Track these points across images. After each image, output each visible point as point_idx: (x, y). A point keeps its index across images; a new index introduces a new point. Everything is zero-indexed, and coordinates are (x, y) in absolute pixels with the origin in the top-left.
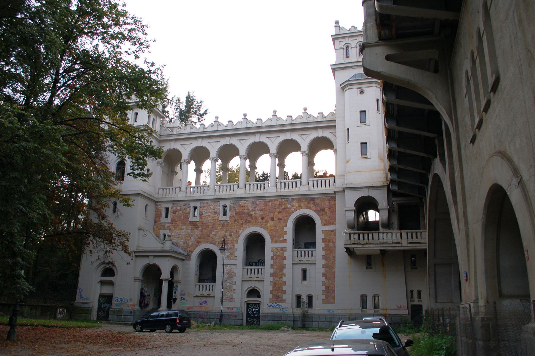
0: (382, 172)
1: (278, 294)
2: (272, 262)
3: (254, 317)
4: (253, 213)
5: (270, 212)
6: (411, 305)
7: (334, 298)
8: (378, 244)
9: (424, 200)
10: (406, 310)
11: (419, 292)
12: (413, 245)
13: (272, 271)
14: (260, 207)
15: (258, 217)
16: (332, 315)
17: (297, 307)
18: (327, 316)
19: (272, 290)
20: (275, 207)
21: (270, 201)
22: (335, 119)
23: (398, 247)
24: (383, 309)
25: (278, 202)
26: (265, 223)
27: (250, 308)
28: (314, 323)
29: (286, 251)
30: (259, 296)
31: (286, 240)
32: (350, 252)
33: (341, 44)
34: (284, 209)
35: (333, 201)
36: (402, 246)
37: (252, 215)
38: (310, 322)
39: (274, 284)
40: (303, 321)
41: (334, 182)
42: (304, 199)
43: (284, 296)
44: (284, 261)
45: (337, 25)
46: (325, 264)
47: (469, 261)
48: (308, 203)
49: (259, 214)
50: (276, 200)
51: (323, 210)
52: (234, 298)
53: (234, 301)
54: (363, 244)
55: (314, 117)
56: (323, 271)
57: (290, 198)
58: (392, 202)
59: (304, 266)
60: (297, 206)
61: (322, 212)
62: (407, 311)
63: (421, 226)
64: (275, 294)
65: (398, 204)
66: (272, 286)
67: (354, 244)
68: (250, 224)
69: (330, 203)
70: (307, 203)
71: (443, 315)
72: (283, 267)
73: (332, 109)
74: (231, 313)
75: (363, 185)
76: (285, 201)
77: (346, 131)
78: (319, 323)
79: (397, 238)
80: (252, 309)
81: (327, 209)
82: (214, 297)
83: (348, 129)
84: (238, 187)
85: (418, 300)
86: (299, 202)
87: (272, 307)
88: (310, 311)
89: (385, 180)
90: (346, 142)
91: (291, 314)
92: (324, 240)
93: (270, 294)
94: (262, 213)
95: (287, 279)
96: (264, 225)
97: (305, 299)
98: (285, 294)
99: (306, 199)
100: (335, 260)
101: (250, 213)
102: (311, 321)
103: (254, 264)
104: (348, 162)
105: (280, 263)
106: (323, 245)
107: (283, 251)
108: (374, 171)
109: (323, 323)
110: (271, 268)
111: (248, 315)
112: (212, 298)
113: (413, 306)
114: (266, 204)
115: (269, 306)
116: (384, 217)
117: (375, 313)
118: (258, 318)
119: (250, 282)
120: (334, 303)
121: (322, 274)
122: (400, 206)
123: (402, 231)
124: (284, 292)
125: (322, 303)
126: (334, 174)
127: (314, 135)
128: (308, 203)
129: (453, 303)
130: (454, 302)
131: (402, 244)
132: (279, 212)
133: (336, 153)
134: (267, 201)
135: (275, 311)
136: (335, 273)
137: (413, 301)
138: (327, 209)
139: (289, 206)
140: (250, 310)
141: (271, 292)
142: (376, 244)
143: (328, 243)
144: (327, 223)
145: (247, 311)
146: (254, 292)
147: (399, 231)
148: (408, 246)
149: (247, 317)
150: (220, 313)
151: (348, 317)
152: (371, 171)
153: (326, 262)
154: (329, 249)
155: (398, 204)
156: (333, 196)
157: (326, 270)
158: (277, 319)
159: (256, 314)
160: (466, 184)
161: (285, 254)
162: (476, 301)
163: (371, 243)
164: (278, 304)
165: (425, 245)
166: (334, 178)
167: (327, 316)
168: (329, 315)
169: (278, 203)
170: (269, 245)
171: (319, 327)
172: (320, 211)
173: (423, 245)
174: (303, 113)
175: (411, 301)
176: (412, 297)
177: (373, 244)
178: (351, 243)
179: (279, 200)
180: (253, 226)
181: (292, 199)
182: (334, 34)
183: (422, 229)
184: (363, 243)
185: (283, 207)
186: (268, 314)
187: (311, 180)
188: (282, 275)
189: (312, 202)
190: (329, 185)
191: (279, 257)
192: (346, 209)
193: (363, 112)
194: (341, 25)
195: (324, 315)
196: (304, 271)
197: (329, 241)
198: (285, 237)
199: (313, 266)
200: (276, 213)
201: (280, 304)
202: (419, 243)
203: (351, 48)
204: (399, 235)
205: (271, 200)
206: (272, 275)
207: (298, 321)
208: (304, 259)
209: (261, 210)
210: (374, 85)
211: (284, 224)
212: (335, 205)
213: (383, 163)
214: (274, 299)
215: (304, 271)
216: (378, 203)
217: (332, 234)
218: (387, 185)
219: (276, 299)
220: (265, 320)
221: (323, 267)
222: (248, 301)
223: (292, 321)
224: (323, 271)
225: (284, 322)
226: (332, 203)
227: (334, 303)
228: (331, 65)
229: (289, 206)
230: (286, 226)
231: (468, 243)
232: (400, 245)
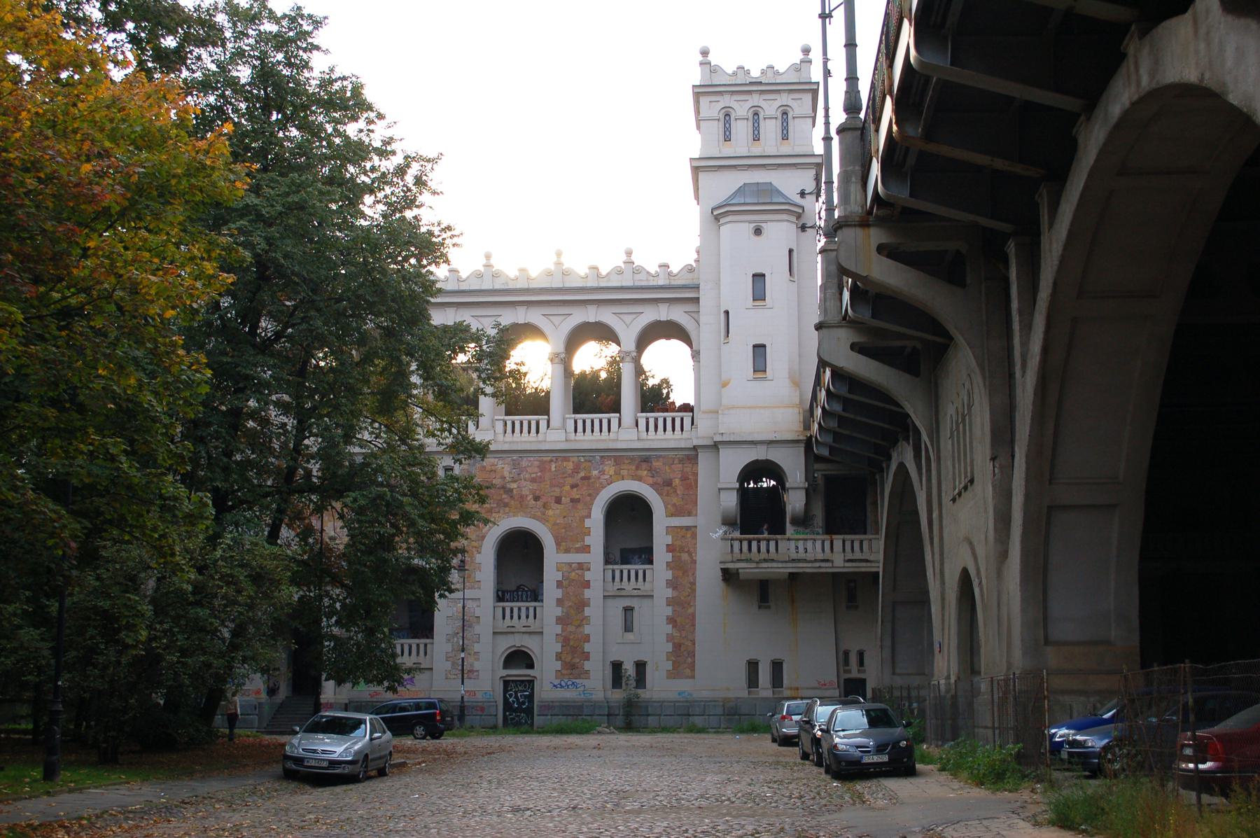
0: (796, 410)
1: (574, 661)
2: (559, 593)
3: (519, 710)
4: (514, 486)
5: (552, 485)
6: (845, 680)
7: (692, 667)
8: (786, 562)
9: (877, 477)
10: (835, 689)
11: (861, 655)
12: (854, 564)
13: (559, 611)
14: (531, 474)
15: (527, 496)
16: (687, 702)
17: (614, 687)
18: (677, 704)
19: (561, 653)
20: (563, 474)
21: (552, 461)
22: (696, 282)
23: (826, 568)
24: (791, 689)
25: (571, 463)
26: (542, 509)
27: (511, 690)
28: (650, 718)
29: (589, 570)
30: (531, 666)
31: (589, 546)
32: (729, 576)
33: (713, 108)
34: (583, 478)
35: (690, 465)
36: (833, 567)
37: (511, 490)
38: (642, 718)
39: (565, 641)
40: (628, 715)
41: (693, 424)
42: (628, 457)
43: (587, 665)
44: (586, 591)
46: (673, 598)
47: (943, 629)
48: (637, 468)
49: (527, 488)
50: (566, 459)
51: (669, 483)
52: (477, 671)
53: (477, 678)
54: (757, 563)
55: (648, 272)
56: (669, 611)
57: (598, 455)
58: (814, 473)
59: (627, 602)
60: (612, 472)
61: (666, 488)
62: (837, 691)
63: (869, 528)
64: (568, 660)
65: (825, 476)
66: (560, 645)
67: (739, 561)
68: (507, 509)
69: (685, 469)
70: (634, 467)
71: (909, 698)
72: (583, 604)
73: (690, 259)
74: (472, 702)
75: (757, 438)
76: (586, 461)
77: (723, 316)
78: (662, 717)
79: (823, 550)
80: (516, 693)
81: (677, 482)
82: (432, 669)
83: (727, 313)
84: (477, 427)
85: (859, 670)
86: (617, 464)
87: (562, 687)
88: (644, 694)
89: (802, 429)
90: (722, 342)
91: (602, 702)
92: (670, 548)
93: (557, 660)
94: (535, 486)
95: (593, 629)
96: (539, 514)
97: (629, 669)
98: (589, 660)
99: (632, 459)
100: (694, 591)
101: (508, 486)
102: (643, 715)
103: (507, 596)
104: (724, 385)
105: (576, 596)
106: (669, 557)
107: (582, 569)
108: (779, 407)
109: (669, 717)
110: (558, 605)
111: (507, 706)
112: (428, 673)
113: (847, 681)
114: (543, 467)
115: (555, 686)
116: (798, 505)
117: (776, 696)
118: (529, 711)
119: (510, 636)
120: (693, 677)
121: (667, 619)
122: (828, 479)
123: (834, 537)
124: (587, 657)
125: (667, 678)
126: (692, 403)
127: (650, 315)
128: (637, 468)
129: (924, 674)
130: (926, 673)
131: (833, 562)
132: (573, 487)
133: (696, 355)
134: (546, 461)
135: (568, 696)
136: (693, 615)
137: (849, 671)
138: (677, 482)
139: (595, 473)
140: (511, 695)
141: (558, 657)
142: (782, 562)
143: (678, 554)
144: (676, 512)
145: (505, 699)
146: (519, 658)
147: (827, 537)
148: (844, 567)
149: (505, 710)
150: (459, 704)
151: (721, 704)
152: (774, 407)
153: (676, 594)
154: (683, 567)
155: (825, 476)
156: (691, 455)
157: (674, 611)
158: (572, 713)
159: (523, 703)
160: (945, 536)
161: (588, 576)
162: (948, 677)
163: (773, 560)
164: (574, 681)
165: (877, 565)
166: (691, 414)
167: (677, 704)
168: (683, 702)
169: (570, 466)
170: (553, 558)
171: (662, 725)
172: (663, 486)
173: (873, 565)
174: (624, 263)
175: (845, 671)
176: (847, 662)
177: (779, 562)
178: (734, 560)
179: (572, 459)
180: (514, 516)
181: (602, 457)
182: (699, 84)
183: (872, 534)
184: (757, 560)
185: (582, 474)
186: (552, 702)
187: (643, 417)
188: (582, 621)
189: (644, 465)
190: (682, 430)
191: (575, 582)
192: (720, 486)
193: (759, 278)
194: (712, 58)
195: (671, 702)
196: (628, 610)
197: (682, 550)
198: (588, 540)
199: (646, 602)
200: (567, 488)
201: (577, 681)
202: (867, 561)
203: (794, 118)
204: (827, 544)
205: (554, 459)
206: (559, 620)
207: (617, 715)
208: (628, 587)
209: (533, 480)
210: (785, 217)
211: (585, 513)
212: (696, 474)
213: (798, 392)
214: (564, 672)
215: (628, 610)
216: (784, 472)
217: (688, 536)
218: (805, 438)
219: (569, 671)
220: (547, 715)
221: (668, 605)
222: (508, 676)
223: (604, 715)
224: (669, 611)
225: (589, 718)
226: (688, 469)
227: (693, 677)
228: (691, 159)
229: (595, 473)
230: (589, 516)
231: (943, 608)
232: (830, 564)
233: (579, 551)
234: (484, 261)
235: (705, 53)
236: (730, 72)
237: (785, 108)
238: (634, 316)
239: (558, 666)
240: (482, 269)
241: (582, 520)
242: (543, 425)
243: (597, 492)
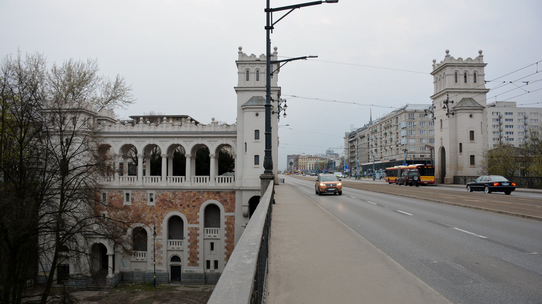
45: (241, 52)
77: (244, 144)
169: (192, 194)
189: (217, 195)
198: (198, 220)
233: (195, 223)
235: (240, 49)
236: (249, 55)
237: (247, 69)
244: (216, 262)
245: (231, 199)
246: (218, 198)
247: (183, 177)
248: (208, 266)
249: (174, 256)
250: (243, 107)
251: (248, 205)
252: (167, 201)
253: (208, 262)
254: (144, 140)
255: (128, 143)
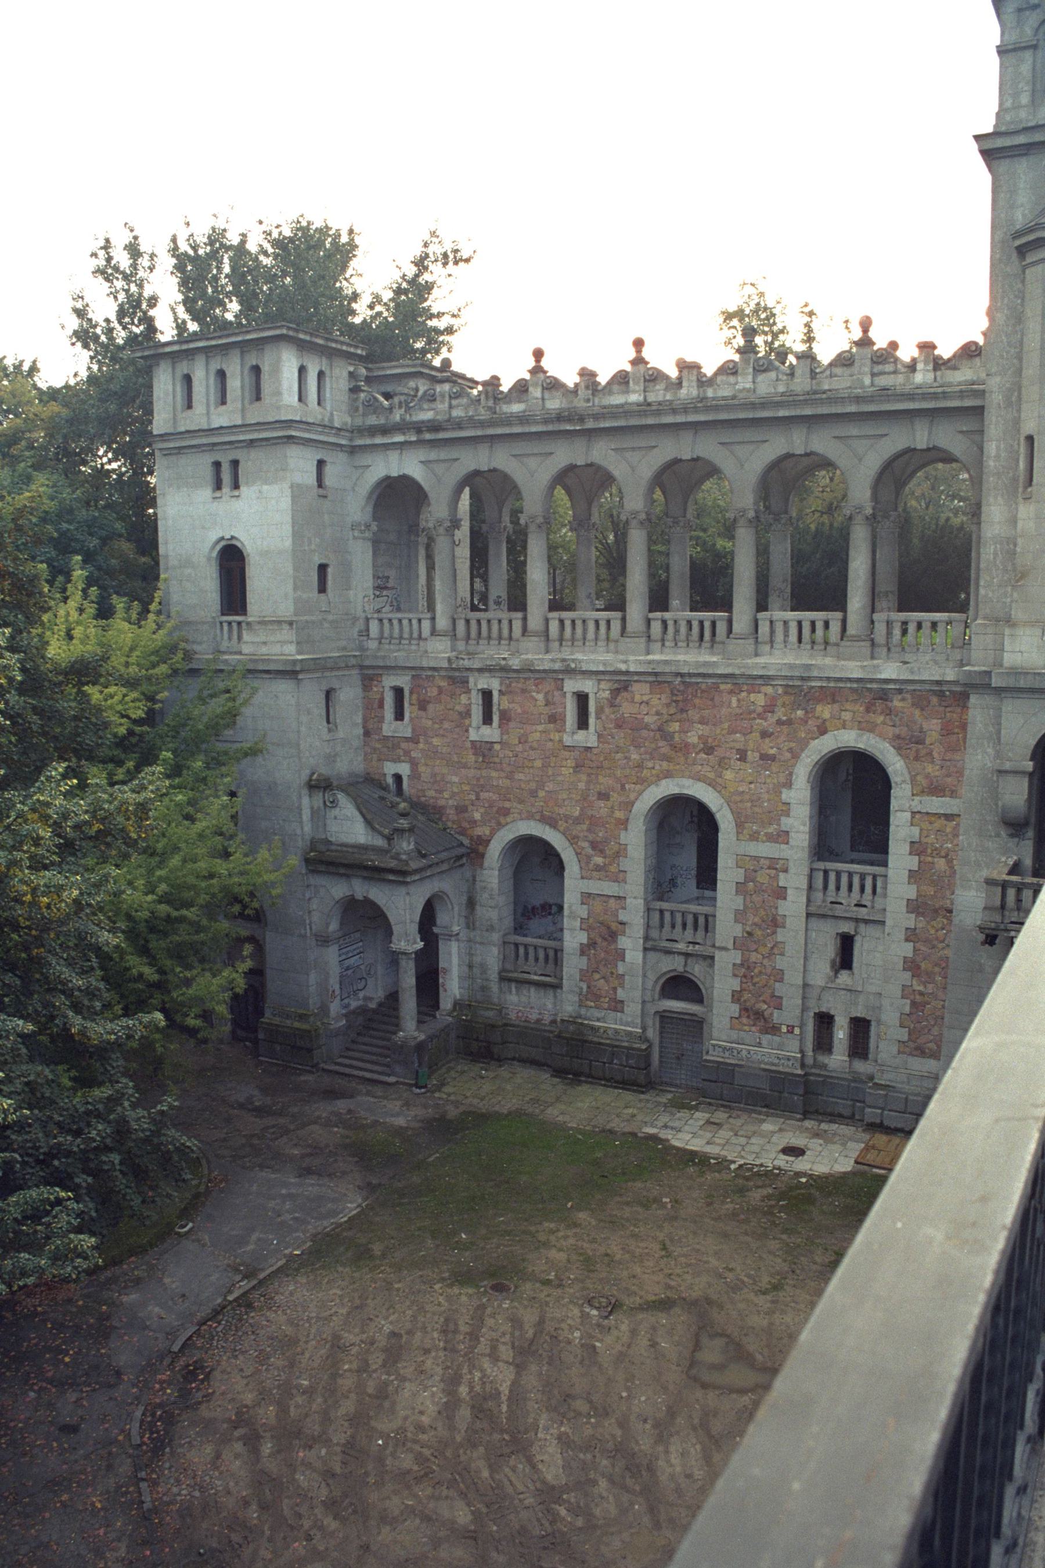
2: (739, 902)
35: (959, 710)
48: (868, 710)
78: (886, 1112)
95: (790, 963)
132: (765, 734)
143: (930, 859)
169: (759, 700)
189: (879, 705)
197: (937, 852)
198: (786, 822)
200: (756, 735)
233: (772, 838)
234: (632, 354)
238: (751, 447)
239: (735, 1009)
240: (628, 368)
241: (777, 791)
242: (721, 628)
243: (804, 744)
244: (860, 1027)
245: (947, 731)
246: (884, 723)
247: (835, 616)
248: (824, 1042)
249: (672, 974)
250: (1018, 243)
251: (1030, 766)
252: (646, 727)
253: (825, 1021)
254: (548, 449)
255: (395, 474)
